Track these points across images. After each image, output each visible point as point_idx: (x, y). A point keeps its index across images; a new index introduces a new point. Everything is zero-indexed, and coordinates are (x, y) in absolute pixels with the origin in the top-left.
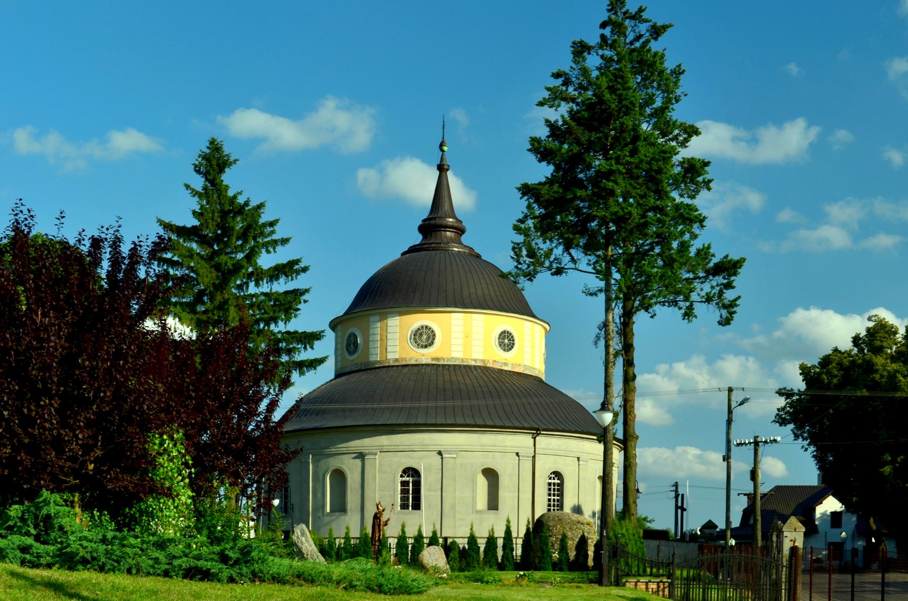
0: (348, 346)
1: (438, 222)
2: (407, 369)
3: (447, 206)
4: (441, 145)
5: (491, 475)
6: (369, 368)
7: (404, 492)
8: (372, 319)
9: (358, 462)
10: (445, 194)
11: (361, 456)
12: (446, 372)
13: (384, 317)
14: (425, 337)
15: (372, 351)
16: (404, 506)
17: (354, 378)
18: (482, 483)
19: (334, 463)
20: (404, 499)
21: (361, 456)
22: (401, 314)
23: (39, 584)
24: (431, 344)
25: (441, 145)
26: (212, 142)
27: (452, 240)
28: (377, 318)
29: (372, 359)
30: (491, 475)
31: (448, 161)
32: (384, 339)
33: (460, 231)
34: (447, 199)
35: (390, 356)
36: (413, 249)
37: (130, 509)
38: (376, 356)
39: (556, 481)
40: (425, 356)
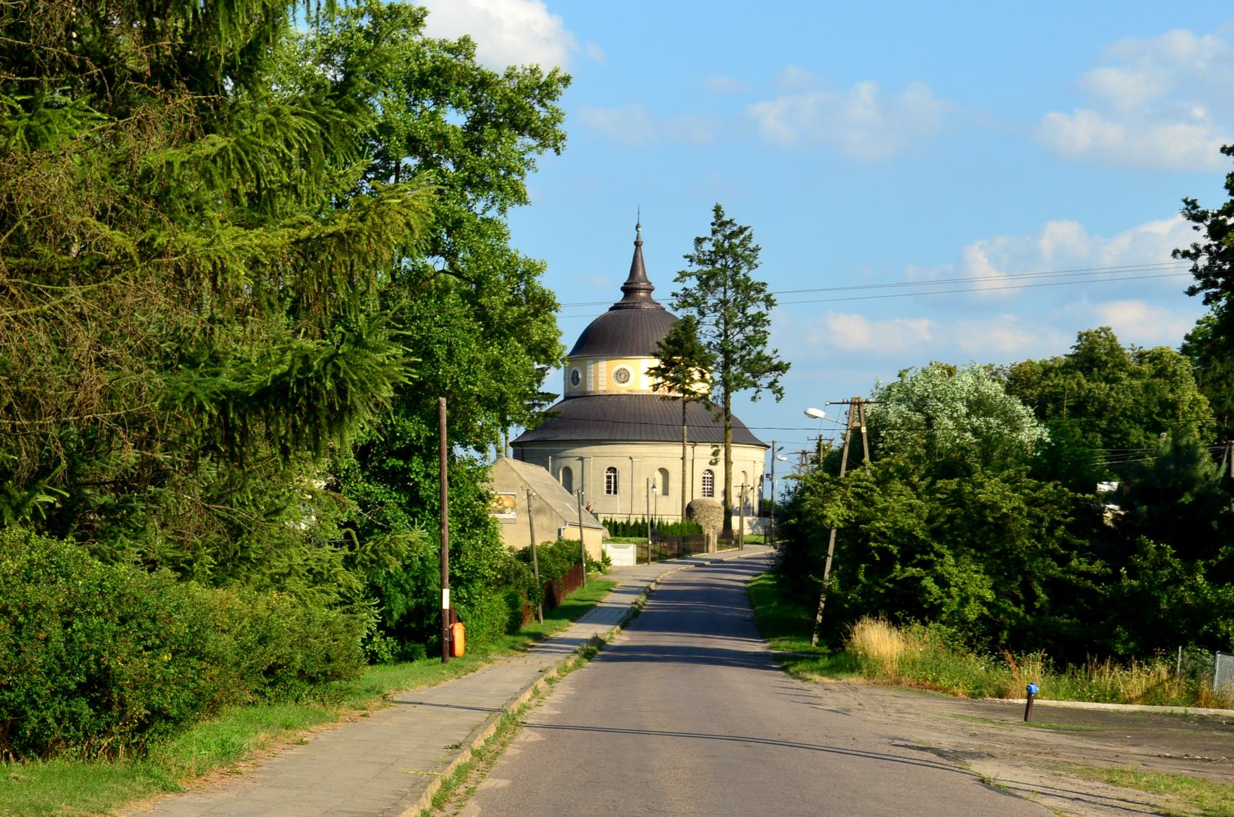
0: (573, 379)
1: (634, 286)
2: (611, 399)
3: (640, 273)
4: (637, 227)
5: (664, 472)
6: (585, 396)
7: (609, 482)
8: (589, 362)
9: (580, 462)
10: (640, 264)
11: (581, 459)
12: (637, 401)
13: (596, 361)
14: (623, 376)
15: (588, 384)
16: (609, 492)
17: (576, 402)
18: (659, 477)
19: (565, 463)
20: (609, 487)
21: (581, 459)
22: (607, 360)
23: (630, 620)
24: (627, 381)
25: (637, 227)
26: (466, 40)
27: (644, 299)
28: (591, 361)
29: (589, 389)
30: (664, 472)
31: (642, 239)
32: (596, 377)
33: (650, 290)
34: (641, 268)
35: (600, 388)
36: (616, 307)
37: (141, 27)
38: (591, 388)
39: (710, 476)
40: (622, 389)
